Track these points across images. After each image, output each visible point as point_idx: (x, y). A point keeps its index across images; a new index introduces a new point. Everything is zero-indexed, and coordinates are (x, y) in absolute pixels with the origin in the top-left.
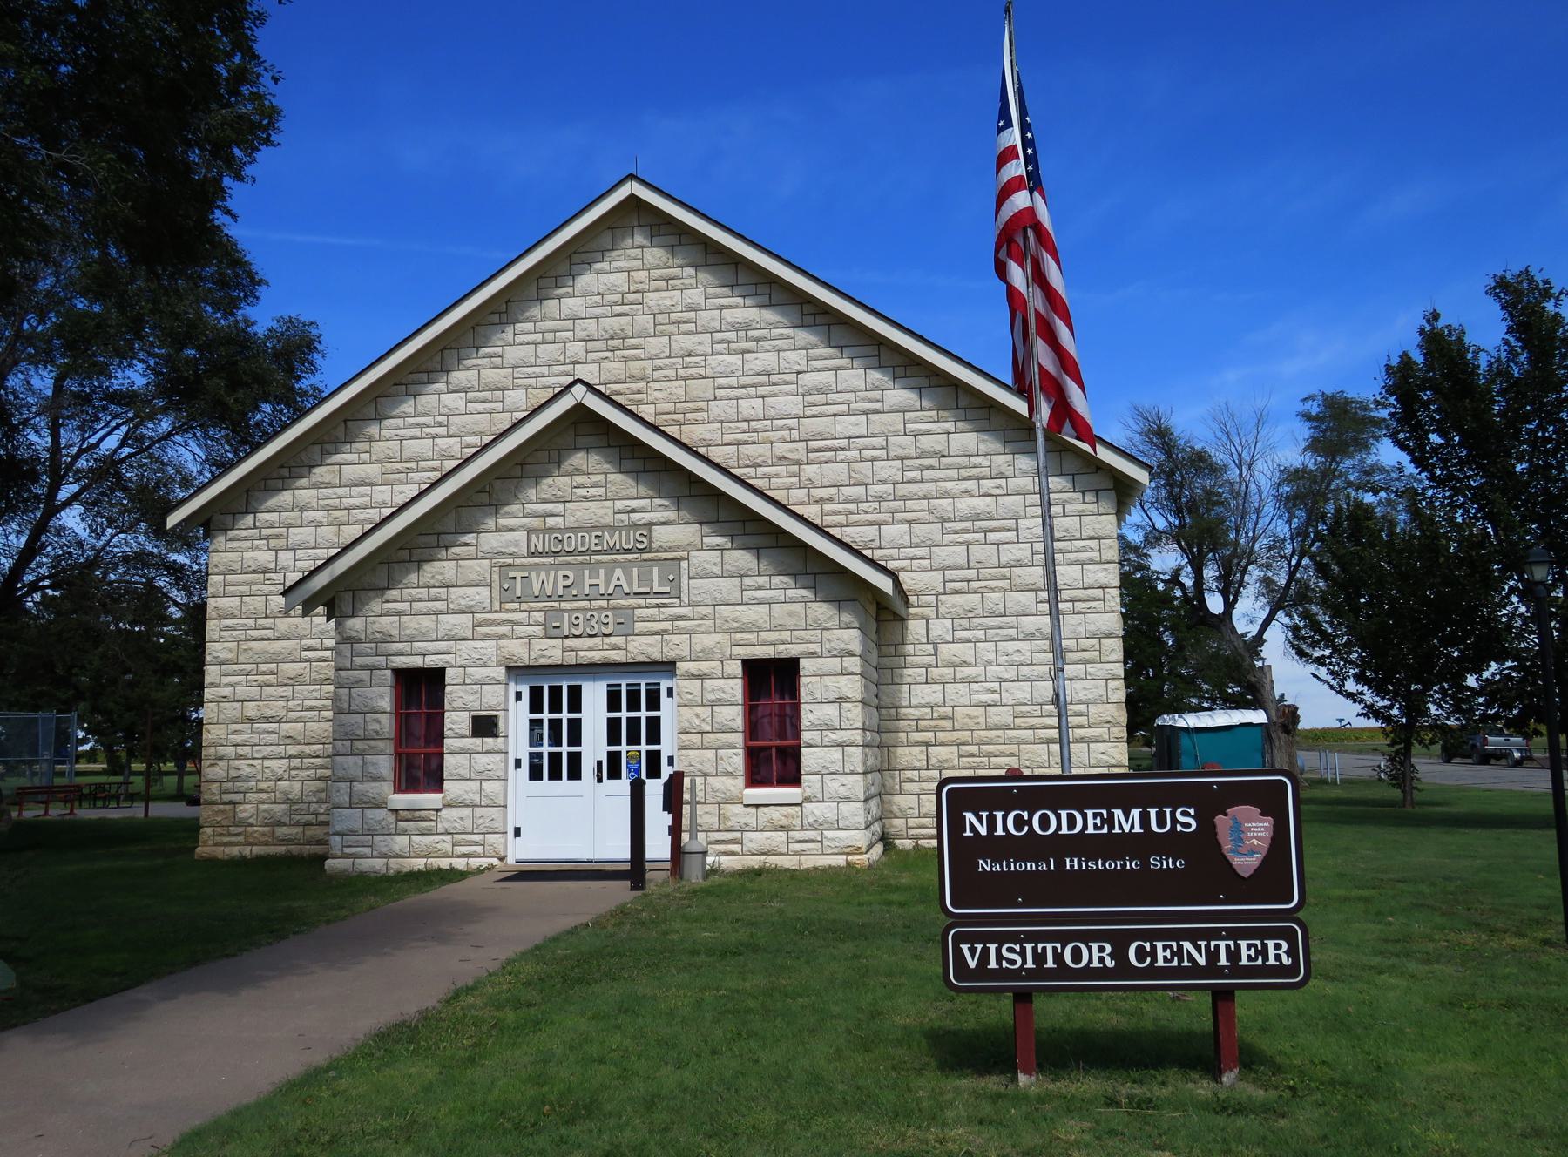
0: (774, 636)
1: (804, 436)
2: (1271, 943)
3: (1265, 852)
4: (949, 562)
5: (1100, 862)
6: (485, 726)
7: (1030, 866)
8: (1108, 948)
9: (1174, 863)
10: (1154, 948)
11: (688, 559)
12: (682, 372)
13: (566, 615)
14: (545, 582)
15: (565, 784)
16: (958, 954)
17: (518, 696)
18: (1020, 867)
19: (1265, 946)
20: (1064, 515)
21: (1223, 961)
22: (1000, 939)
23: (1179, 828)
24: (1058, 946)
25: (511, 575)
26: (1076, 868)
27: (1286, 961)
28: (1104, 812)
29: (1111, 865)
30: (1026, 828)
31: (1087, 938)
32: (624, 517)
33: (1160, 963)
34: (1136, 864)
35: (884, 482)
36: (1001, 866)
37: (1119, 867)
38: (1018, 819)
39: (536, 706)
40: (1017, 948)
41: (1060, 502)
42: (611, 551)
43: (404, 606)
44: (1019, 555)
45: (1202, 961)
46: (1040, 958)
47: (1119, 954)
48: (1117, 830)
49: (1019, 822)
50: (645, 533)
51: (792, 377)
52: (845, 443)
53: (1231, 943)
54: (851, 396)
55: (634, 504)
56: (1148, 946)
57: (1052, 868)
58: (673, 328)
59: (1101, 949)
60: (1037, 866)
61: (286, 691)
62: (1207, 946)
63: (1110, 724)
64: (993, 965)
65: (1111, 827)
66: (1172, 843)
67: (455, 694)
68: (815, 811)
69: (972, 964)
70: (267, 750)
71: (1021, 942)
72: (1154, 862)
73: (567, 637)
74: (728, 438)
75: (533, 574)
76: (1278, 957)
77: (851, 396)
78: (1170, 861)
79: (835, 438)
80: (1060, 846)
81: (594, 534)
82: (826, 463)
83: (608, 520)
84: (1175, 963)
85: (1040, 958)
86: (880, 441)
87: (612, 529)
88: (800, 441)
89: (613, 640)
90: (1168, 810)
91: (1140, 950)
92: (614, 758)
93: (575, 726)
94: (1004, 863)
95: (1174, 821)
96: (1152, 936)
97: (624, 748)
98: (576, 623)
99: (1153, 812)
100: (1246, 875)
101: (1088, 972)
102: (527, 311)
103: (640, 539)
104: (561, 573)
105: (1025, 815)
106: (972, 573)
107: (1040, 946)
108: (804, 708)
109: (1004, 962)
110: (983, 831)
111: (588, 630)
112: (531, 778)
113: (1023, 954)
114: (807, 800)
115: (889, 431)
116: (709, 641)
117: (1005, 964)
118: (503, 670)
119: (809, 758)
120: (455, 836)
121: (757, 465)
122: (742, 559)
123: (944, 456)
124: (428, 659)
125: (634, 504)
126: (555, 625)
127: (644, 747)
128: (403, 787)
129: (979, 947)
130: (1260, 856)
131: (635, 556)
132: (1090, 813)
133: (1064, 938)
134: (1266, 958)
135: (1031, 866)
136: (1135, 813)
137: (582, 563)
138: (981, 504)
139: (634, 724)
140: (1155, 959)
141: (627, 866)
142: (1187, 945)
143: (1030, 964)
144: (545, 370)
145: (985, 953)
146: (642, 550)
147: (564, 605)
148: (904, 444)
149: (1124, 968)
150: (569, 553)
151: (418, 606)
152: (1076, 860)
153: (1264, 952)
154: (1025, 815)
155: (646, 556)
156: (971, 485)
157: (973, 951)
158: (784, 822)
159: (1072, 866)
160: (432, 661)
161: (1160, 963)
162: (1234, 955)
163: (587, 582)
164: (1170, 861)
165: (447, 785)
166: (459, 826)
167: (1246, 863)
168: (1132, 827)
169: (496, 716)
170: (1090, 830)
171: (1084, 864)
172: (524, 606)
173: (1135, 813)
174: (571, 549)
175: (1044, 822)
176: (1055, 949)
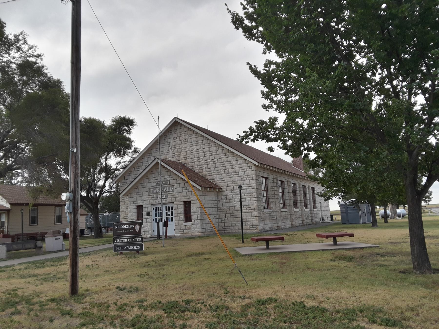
0: (187, 197)
4: (228, 181)
6: (148, 214)
17: (153, 209)
31: (125, 239)
39: (156, 211)
47: (127, 240)
49: (120, 227)
51: (202, 150)
55: (167, 177)
58: (184, 143)
63: (255, 209)
72: (124, 231)
74: (193, 161)
85: (121, 241)
89: (165, 199)
96: (130, 238)
97: (157, 217)
101: (125, 242)
106: (231, 183)
119: (193, 217)
121: (197, 166)
125: (167, 177)
138: (233, 170)
144: (165, 152)
148: (220, 160)
149: (128, 242)
151: (139, 196)
160: (141, 204)
167: (137, 230)
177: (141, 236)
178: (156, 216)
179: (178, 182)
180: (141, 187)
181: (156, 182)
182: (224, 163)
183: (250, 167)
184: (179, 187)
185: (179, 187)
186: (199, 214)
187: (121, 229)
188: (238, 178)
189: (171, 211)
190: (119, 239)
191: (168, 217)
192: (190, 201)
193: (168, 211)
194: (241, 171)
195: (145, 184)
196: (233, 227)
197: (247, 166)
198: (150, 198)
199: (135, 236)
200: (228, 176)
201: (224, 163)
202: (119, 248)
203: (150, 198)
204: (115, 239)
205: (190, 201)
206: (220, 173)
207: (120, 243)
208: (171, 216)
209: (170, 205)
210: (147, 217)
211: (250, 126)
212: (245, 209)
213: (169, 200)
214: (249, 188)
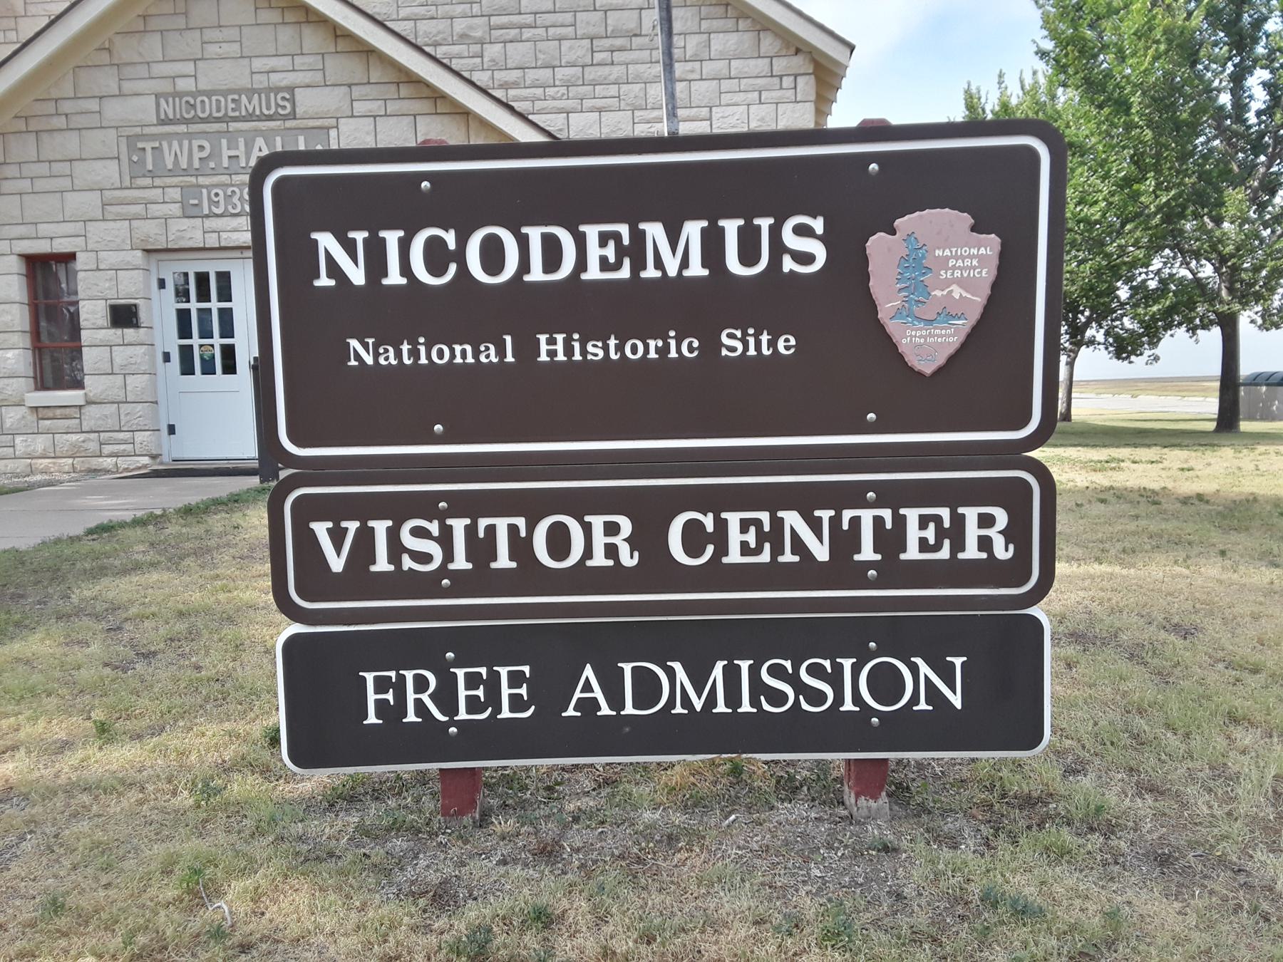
1: (486, 11)
2: (971, 514)
3: (974, 315)
5: (612, 342)
6: (124, 316)
7: (463, 353)
8: (626, 525)
9: (773, 344)
10: (721, 525)
11: (337, 127)
13: (204, 191)
14: (179, 153)
15: (219, 377)
16: (307, 543)
17: (162, 284)
18: (441, 355)
19: (959, 521)
20: (760, 103)
21: (867, 553)
22: (398, 509)
23: (788, 264)
24: (521, 522)
25: (140, 145)
26: (561, 357)
27: (1002, 552)
28: (624, 229)
29: (636, 350)
30: (453, 268)
31: (581, 505)
32: (264, 78)
33: (734, 556)
34: (691, 349)
35: (572, 65)
36: (399, 354)
37: (653, 355)
38: (434, 247)
39: (182, 294)
40: (434, 528)
41: (757, 88)
42: (250, 117)
43: (25, 185)
45: (821, 552)
46: (481, 548)
48: (650, 273)
49: (437, 257)
50: (288, 97)
52: (529, 19)
53: (887, 514)
56: (708, 522)
57: (510, 358)
59: (612, 529)
60: (476, 354)
62: (835, 522)
64: (382, 564)
65: (639, 265)
69: (337, 564)
71: (442, 517)
72: (731, 343)
73: (207, 216)
75: (165, 145)
76: (985, 543)
78: (765, 338)
79: (520, 14)
81: (230, 97)
82: (511, 42)
83: (245, 82)
84: (765, 557)
85: (481, 548)
86: (568, 18)
87: (251, 92)
88: (482, 16)
90: (765, 223)
91: (692, 529)
93: (226, 316)
94: (405, 347)
95: (778, 248)
96: (717, 501)
98: (216, 199)
99: (731, 227)
100: (928, 369)
101: (583, 578)
103: (281, 103)
104: (196, 143)
105: (450, 238)
107: (483, 523)
109: (406, 558)
110: (357, 276)
111: (230, 208)
112: (184, 373)
113: (445, 539)
115: (579, 6)
117: (407, 563)
118: (139, 253)
120: (102, 434)
123: (635, 35)
124: (56, 242)
126: (193, 202)
128: (50, 382)
129: (352, 526)
130: (963, 326)
131: (278, 123)
132: (592, 232)
133: (534, 507)
134: (959, 545)
135: (464, 353)
136: (693, 230)
137: (219, 132)
140: (722, 549)
141: (255, 464)
142: (792, 519)
143: (461, 562)
145: (365, 539)
147: (201, 180)
150: (204, 121)
151: (40, 185)
152: (560, 338)
153: (956, 534)
154: (450, 238)
155: (289, 124)
157: (337, 536)
159: (552, 354)
160: (62, 246)
161: (734, 556)
162: (890, 540)
163: (226, 153)
164: (765, 338)
165: (88, 381)
168: (685, 263)
169: (135, 305)
170: (593, 273)
171: (577, 345)
172: (158, 182)
173: (693, 230)
174: (205, 115)
175: (493, 255)
176: (513, 529)
177: (1011, 454)
178: (185, 331)
179: (360, 107)
180: (60, 122)
181: (177, 94)
182: (619, 42)
183: (788, 82)
190: (424, 506)
194: (726, 98)
195: (93, 105)
198: (138, 209)
201: (619, 42)
203: (138, 209)
204: (308, 510)
206: (588, 103)
207: (463, 583)
210: (115, 334)
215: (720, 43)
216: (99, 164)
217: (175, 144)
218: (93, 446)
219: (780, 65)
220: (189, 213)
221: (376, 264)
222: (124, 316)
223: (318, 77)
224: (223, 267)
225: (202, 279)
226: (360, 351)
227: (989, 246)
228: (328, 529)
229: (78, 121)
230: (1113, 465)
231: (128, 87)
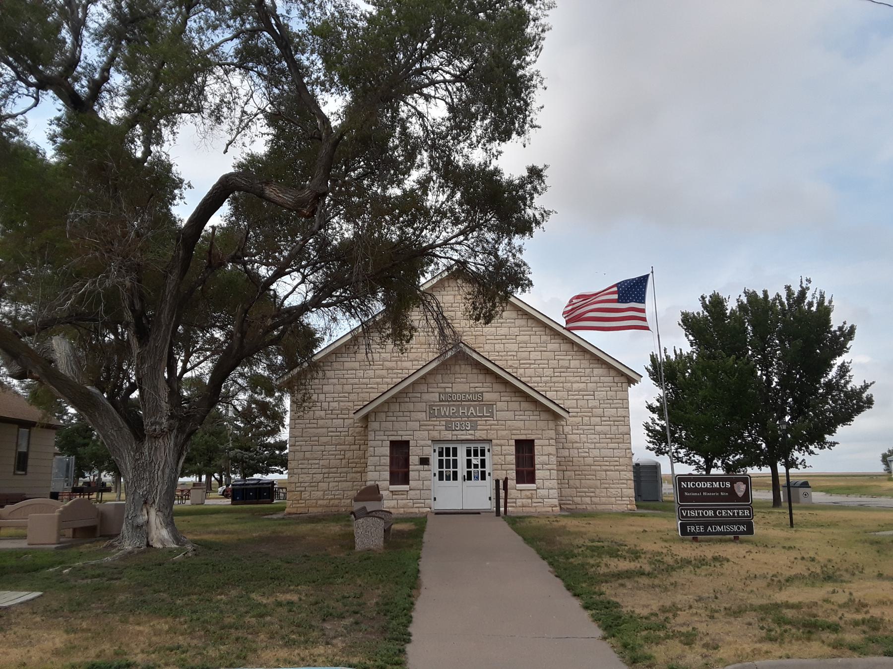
0: (526, 432)
6: (424, 461)
12: (474, 333)
17: (435, 451)
18: (694, 494)
22: (690, 510)
31: (708, 509)
39: (441, 454)
42: (469, 401)
44: (595, 404)
46: (698, 514)
47: (715, 513)
49: (693, 485)
54: (535, 345)
55: (477, 385)
61: (322, 448)
66: (725, 490)
67: (413, 450)
68: (541, 492)
70: (314, 471)
72: (704, 494)
77: (535, 345)
80: (702, 490)
85: (698, 514)
86: (546, 362)
87: (469, 393)
89: (470, 432)
92: (469, 473)
93: (455, 461)
96: (721, 509)
97: (444, 470)
101: (709, 517)
102: (44, 158)
106: (579, 410)
108: (536, 457)
114: (538, 488)
116: (504, 433)
119: (538, 474)
122: (514, 405)
125: (477, 385)
127: (452, 470)
133: (703, 510)
138: (582, 386)
139: (448, 461)
146: (478, 399)
148: (553, 363)
149: (716, 516)
150: (454, 401)
156: (578, 378)
158: (530, 496)
160: (405, 438)
163: (461, 411)
166: (416, 497)
167: (740, 494)
175: (699, 485)
177: (749, 505)
178: (441, 466)
180: (408, 400)
181: (445, 393)
182: (562, 370)
184: (506, 409)
185: (506, 409)
186: (555, 468)
187: (696, 490)
188: (592, 403)
189: (480, 457)
190: (693, 509)
191: (472, 469)
192: (533, 441)
193: (472, 458)
196: (579, 499)
197: (612, 381)
198: (432, 427)
199: (690, 505)
200: (570, 397)
201: (562, 370)
202: (693, 529)
205: (533, 441)
207: (697, 517)
208: (480, 469)
209: (479, 446)
211: (683, 313)
212: (607, 463)
213: (480, 434)
214: (616, 423)
215: (596, 371)
216: (419, 413)
217: (445, 409)
218: (411, 504)
219: (616, 379)
220: (448, 429)
221: (687, 485)
222: (424, 461)
223: (490, 390)
224: (454, 446)
225: (448, 449)
226: (686, 494)
227: (745, 486)
228: (798, 502)
229: (414, 400)
230: (98, 572)
231: (430, 390)
